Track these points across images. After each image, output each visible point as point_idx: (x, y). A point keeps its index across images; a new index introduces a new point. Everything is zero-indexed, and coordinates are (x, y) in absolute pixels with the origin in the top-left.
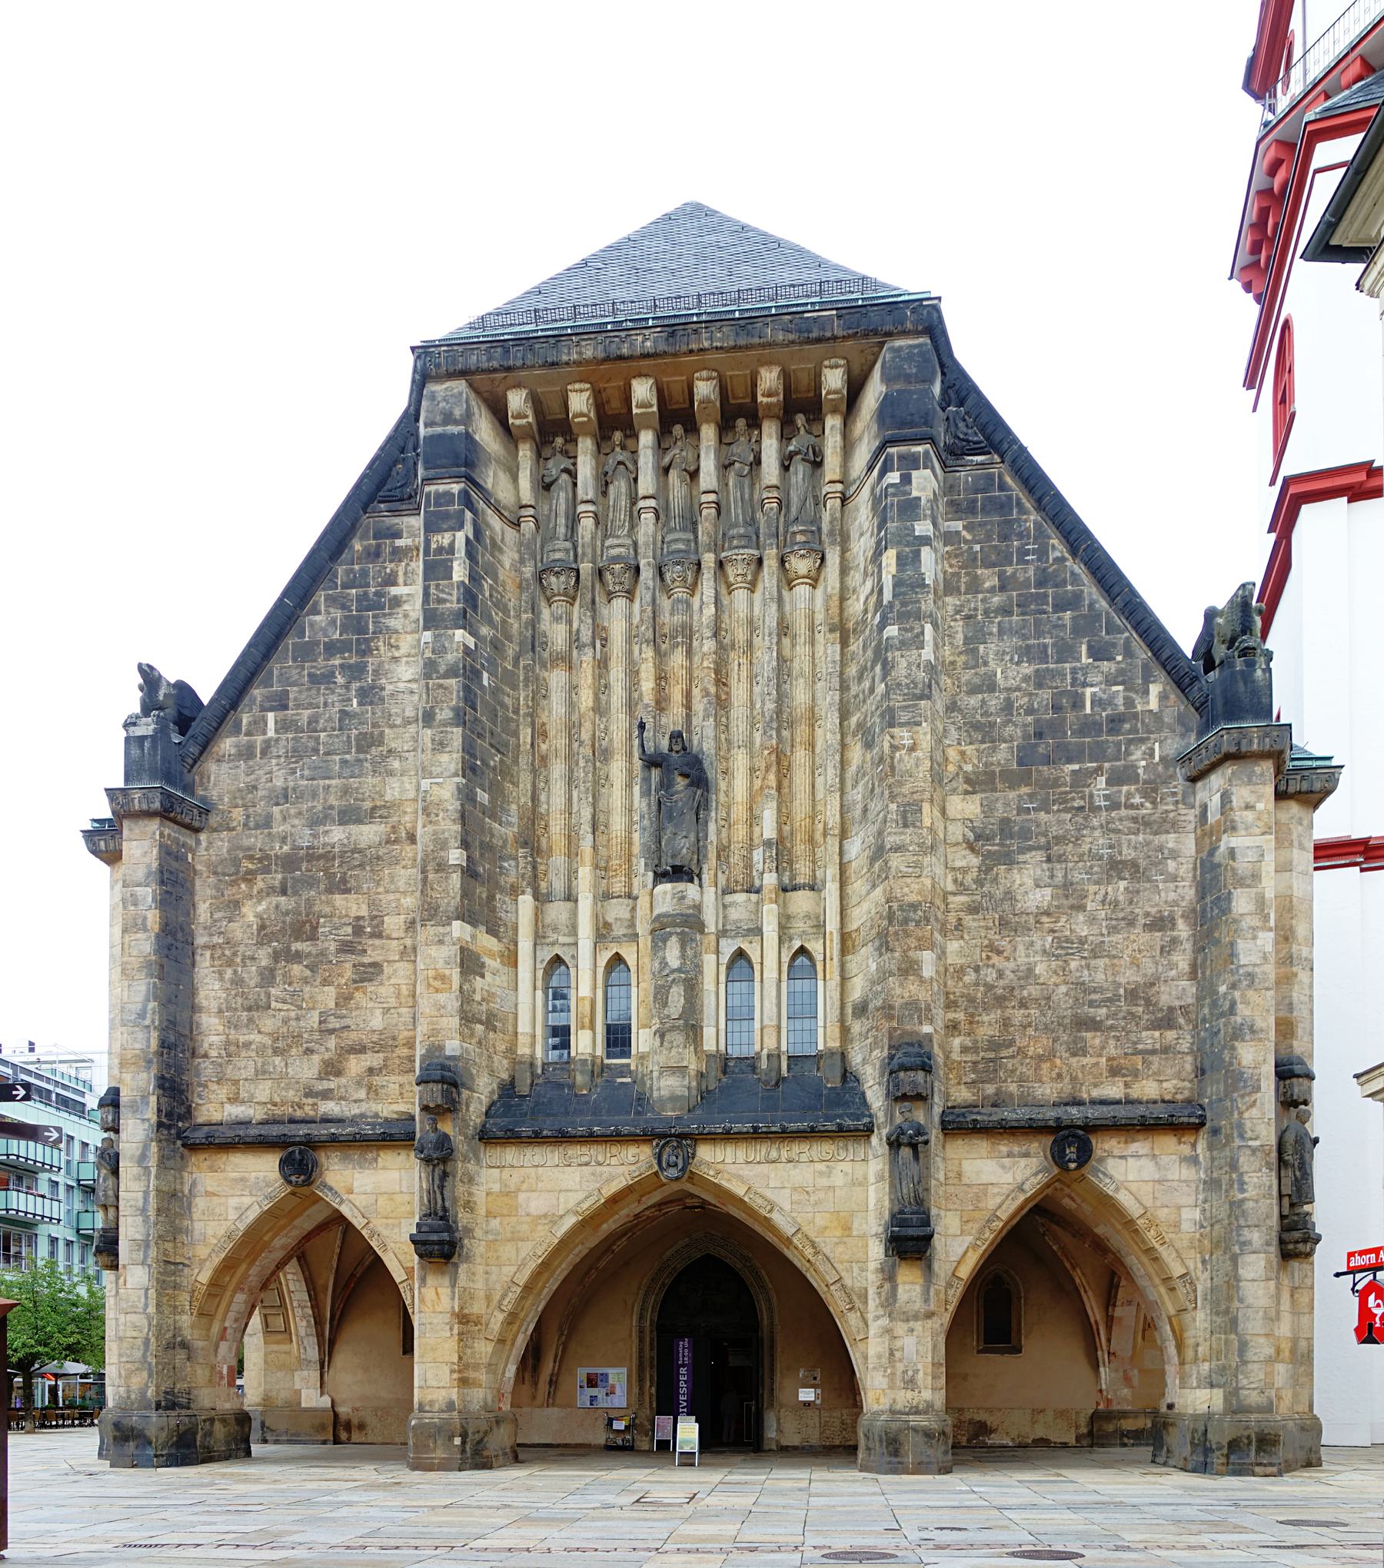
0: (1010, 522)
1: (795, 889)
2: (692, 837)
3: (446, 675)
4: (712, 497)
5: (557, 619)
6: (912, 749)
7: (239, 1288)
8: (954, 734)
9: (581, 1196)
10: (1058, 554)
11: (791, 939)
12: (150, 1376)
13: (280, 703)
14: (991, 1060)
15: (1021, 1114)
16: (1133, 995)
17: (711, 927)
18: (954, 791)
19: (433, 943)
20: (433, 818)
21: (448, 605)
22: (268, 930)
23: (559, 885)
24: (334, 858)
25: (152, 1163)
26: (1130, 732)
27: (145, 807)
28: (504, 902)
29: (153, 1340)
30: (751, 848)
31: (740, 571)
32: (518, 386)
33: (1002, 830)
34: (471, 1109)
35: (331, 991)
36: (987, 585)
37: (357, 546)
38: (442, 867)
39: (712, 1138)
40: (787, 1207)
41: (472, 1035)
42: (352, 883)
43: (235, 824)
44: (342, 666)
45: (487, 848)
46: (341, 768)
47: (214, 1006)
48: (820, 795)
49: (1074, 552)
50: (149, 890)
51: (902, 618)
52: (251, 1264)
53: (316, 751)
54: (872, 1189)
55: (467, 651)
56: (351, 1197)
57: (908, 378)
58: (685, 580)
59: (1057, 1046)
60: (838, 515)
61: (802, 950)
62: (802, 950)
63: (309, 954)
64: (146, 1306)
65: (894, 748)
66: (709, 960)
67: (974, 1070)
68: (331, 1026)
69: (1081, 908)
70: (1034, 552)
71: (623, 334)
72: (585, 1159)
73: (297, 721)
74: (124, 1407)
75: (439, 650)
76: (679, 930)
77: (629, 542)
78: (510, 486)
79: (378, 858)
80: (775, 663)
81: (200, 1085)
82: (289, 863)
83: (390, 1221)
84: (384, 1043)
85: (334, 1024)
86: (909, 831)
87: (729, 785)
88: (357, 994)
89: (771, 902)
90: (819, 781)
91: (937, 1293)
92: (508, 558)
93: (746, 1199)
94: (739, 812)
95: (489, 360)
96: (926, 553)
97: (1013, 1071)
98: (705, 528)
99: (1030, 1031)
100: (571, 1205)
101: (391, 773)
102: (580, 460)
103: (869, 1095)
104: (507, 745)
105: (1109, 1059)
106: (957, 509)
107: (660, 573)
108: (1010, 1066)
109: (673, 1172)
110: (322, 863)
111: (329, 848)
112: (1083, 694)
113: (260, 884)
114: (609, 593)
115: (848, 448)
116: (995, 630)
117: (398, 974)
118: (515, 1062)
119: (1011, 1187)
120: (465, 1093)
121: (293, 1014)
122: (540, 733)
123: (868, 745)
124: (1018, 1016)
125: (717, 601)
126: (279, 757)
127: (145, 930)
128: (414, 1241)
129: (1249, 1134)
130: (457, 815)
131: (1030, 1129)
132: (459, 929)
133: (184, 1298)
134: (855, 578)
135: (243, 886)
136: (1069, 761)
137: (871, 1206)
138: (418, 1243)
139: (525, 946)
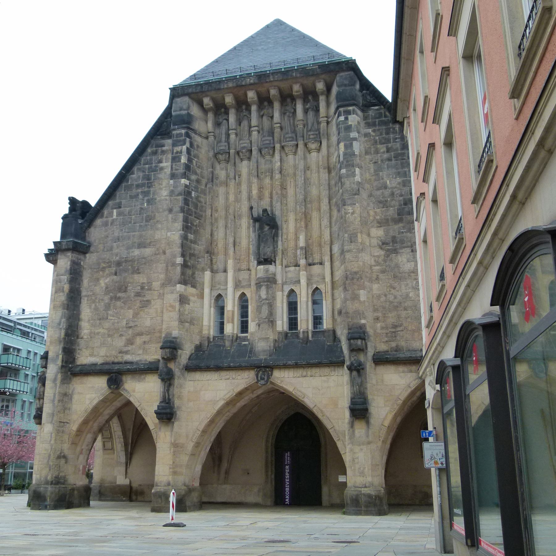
1: (314, 264)
2: (271, 248)
3: (178, 195)
4: (278, 125)
5: (222, 169)
6: (353, 213)
8: (371, 204)
11: (312, 284)
12: (50, 470)
14: (394, 332)
17: (279, 281)
18: (373, 227)
21: (179, 171)
23: (221, 266)
24: (135, 262)
25: (58, 382)
28: (199, 275)
29: (52, 455)
30: (296, 249)
31: (290, 149)
32: (207, 96)
33: (393, 241)
34: (182, 357)
35: (131, 312)
36: (382, 151)
38: (174, 264)
42: (141, 270)
44: (142, 192)
45: (192, 255)
51: (347, 166)
52: (94, 422)
53: (130, 222)
54: (345, 387)
55: (186, 186)
56: (134, 394)
57: (345, 85)
58: (269, 153)
60: (326, 128)
64: (51, 440)
65: (346, 213)
66: (279, 294)
67: (387, 336)
68: (130, 325)
70: (399, 138)
71: (243, 79)
72: (228, 377)
74: (38, 485)
76: (266, 284)
77: (248, 141)
79: (151, 260)
80: (303, 182)
82: (119, 264)
85: (131, 324)
87: (288, 226)
90: (322, 223)
94: (291, 236)
95: (196, 90)
96: (355, 143)
97: (403, 336)
98: (276, 135)
99: (409, 320)
101: (157, 229)
102: (230, 116)
104: (202, 216)
106: (368, 125)
107: (260, 151)
108: (401, 335)
109: (262, 382)
110: (130, 263)
111: (133, 258)
113: (107, 271)
114: (241, 159)
115: (328, 104)
116: (386, 166)
117: (156, 304)
120: (180, 352)
121: (116, 321)
122: (214, 210)
123: (339, 211)
126: (117, 225)
127: (63, 292)
128: (156, 412)
130: (179, 245)
133: (66, 437)
134: (332, 150)
135: (101, 273)
137: (345, 395)
139: (207, 291)
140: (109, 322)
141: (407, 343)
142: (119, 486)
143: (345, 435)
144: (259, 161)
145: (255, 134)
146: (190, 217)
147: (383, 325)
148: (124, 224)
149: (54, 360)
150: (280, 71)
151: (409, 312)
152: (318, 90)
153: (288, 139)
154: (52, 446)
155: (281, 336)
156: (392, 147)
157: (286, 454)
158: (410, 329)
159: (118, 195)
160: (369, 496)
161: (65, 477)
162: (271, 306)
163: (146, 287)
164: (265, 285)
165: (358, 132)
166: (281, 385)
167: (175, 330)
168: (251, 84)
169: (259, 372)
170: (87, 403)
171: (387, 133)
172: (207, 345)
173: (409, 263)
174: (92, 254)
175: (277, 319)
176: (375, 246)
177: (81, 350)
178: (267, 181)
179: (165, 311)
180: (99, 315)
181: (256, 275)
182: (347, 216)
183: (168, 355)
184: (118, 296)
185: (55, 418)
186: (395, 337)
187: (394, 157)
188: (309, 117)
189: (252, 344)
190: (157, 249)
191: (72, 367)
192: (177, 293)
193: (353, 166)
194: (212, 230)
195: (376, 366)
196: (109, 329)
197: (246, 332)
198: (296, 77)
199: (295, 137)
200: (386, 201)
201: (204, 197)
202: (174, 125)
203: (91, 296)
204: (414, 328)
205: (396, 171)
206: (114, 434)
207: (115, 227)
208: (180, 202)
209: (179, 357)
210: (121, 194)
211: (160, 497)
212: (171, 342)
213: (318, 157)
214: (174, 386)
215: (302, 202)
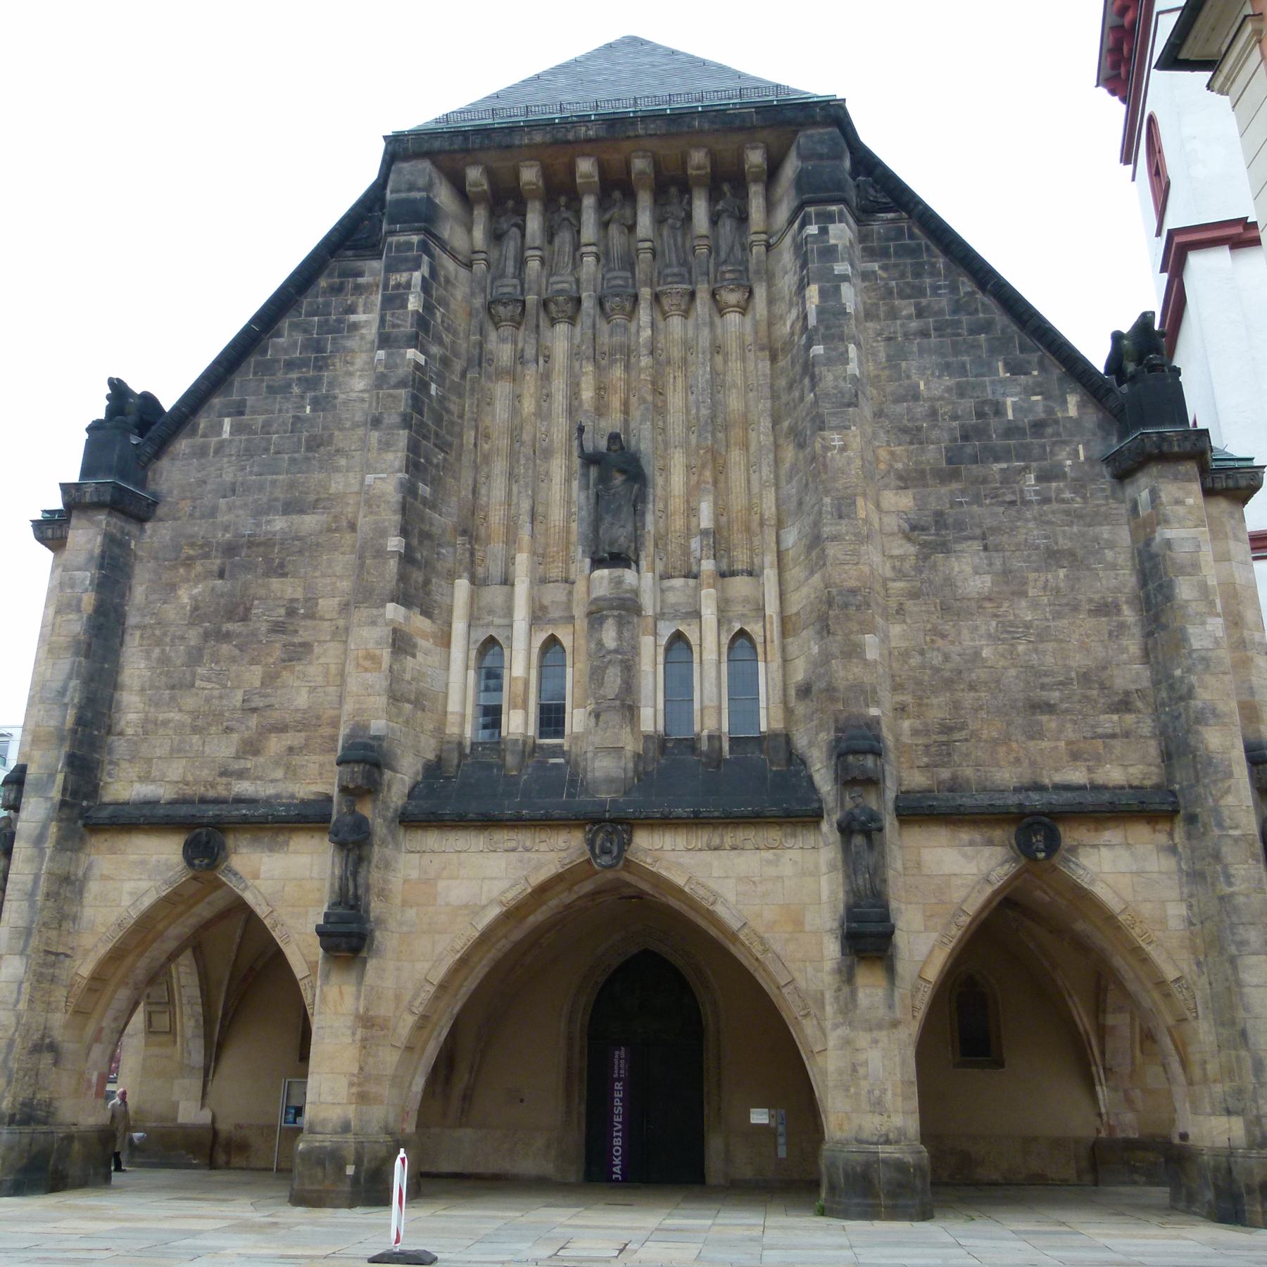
1: (733, 574)
2: (630, 528)
3: (396, 386)
4: (648, 244)
5: (503, 340)
6: (843, 449)
8: (883, 436)
9: (504, 884)
11: (730, 621)
12: (9, 1083)
14: (943, 743)
16: (1085, 678)
17: (649, 611)
18: (886, 487)
20: (375, 509)
21: (402, 329)
23: (496, 570)
24: (274, 545)
26: (1053, 436)
27: (95, 499)
28: (440, 586)
30: (688, 534)
31: (675, 302)
32: (476, 163)
33: (937, 522)
35: (258, 670)
36: (904, 313)
38: (381, 553)
40: (732, 898)
41: (399, 714)
42: (290, 568)
44: (299, 379)
45: (426, 536)
46: (289, 465)
48: (755, 490)
51: (826, 340)
52: (141, 955)
53: (267, 450)
55: (417, 366)
56: (257, 882)
58: (623, 308)
62: (742, 633)
63: (239, 635)
64: (17, 1001)
65: (826, 448)
66: (647, 642)
67: (927, 753)
68: (253, 705)
69: (1023, 594)
70: (945, 287)
71: (569, 126)
72: (512, 844)
76: (616, 613)
77: (572, 279)
78: (465, 237)
79: (318, 545)
82: (230, 550)
84: (308, 722)
85: (258, 702)
86: (844, 522)
87: (667, 481)
93: (687, 889)
94: (677, 504)
95: (451, 144)
97: (967, 755)
99: (983, 714)
100: (495, 893)
101: (337, 470)
104: (450, 445)
105: (1069, 743)
106: (870, 253)
107: (601, 302)
108: (964, 749)
109: (606, 860)
110: (262, 549)
111: (270, 536)
112: (1005, 403)
113: (198, 568)
115: (770, 207)
116: (915, 349)
117: (327, 655)
120: (388, 774)
121: (216, 693)
124: (968, 699)
125: (653, 325)
126: (231, 455)
127: (79, 610)
128: (320, 931)
129: (1228, 822)
130: (397, 507)
132: (393, 611)
133: (60, 994)
135: (182, 570)
136: (997, 459)
139: (459, 627)
140: (197, 694)
141: (978, 770)
142: (183, 1127)
143: (823, 1003)
144: (598, 326)
145: (589, 261)
146: (424, 442)
147: (918, 724)
148: (248, 452)
149: (42, 787)
150: (663, 113)
151: (983, 694)
152: (750, 167)
153: (669, 279)
154: (19, 1017)
155: (651, 746)
156: (929, 306)
157: (617, 1053)
158: (984, 737)
159: (236, 384)
160: (900, 1166)
161: (49, 1104)
162: (629, 668)
163: (302, 611)
164: (614, 616)
165: (852, 266)
166: (654, 870)
167: (378, 718)
168: (589, 140)
169: (595, 834)
170: (123, 904)
171: (917, 275)
172: (455, 762)
173: (977, 577)
174: (160, 524)
175: (643, 703)
176: (893, 534)
177: (117, 764)
178: (618, 372)
179: (350, 668)
180: (171, 677)
181: (588, 592)
182: (829, 454)
183: (360, 781)
184: (224, 629)
185: (34, 942)
186: (949, 754)
187: (935, 329)
188: (722, 231)
189: (577, 764)
190: (335, 517)
191: (89, 808)
192: (387, 625)
193: (841, 339)
194: (475, 481)
195: (901, 827)
196: (195, 715)
197: (559, 733)
198: (701, 132)
199: (687, 276)
200: (919, 429)
201: (457, 400)
202: (392, 221)
203: (151, 626)
204: (995, 734)
205: (939, 360)
206: (180, 993)
207: (225, 460)
208: (403, 403)
209: (386, 789)
210: (245, 381)
211: (321, 1163)
212: (366, 747)
213: (742, 324)
214: (370, 862)
215: (706, 423)
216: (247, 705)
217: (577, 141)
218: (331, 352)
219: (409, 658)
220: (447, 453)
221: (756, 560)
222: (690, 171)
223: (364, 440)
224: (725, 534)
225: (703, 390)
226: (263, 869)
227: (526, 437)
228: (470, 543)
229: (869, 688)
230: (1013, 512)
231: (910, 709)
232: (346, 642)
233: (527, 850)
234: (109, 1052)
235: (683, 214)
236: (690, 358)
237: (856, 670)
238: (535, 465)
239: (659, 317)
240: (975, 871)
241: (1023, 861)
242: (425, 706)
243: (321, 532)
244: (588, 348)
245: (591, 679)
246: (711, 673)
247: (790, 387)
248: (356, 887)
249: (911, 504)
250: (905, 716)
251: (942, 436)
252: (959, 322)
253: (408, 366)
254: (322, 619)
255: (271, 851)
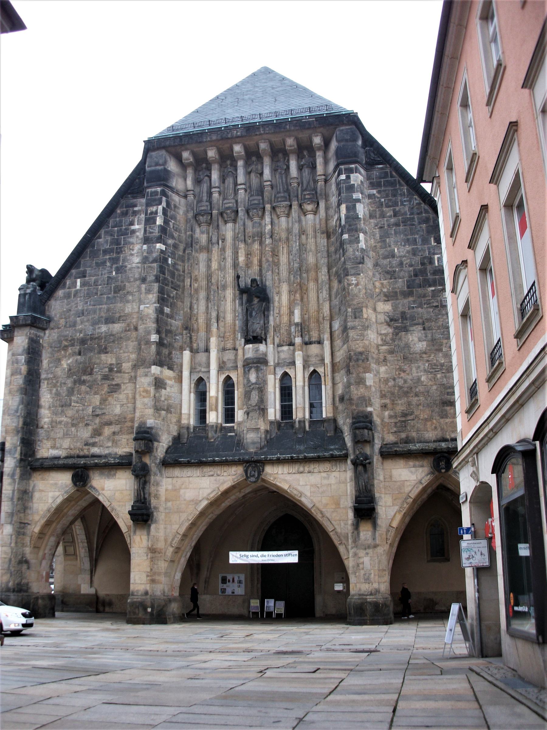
0: (396, 190)
1: (311, 343)
2: (262, 322)
4: (269, 183)
5: (202, 233)
6: (357, 285)
7: (52, 535)
8: (378, 276)
9: (209, 491)
10: (417, 202)
11: (309, 367)
12: (11, 576)
13: (83, 275)
15: (418, 446)
17: (271, 363)
18: (379, 300)
19: (143, 376)
20: (145, 322)
22: (72, 371)
23: (202, 345)
24: (102, 339)
25: (17, 477)
27: (24, 323)
28: (177, 354)
30: (290, 325)
31: (282, 210)
32: (186, 149)
33: (402, 317)
36: (388, 214)
37: (119, 211)
38: (148, 342)
39: (273, 462)
40: (308, 494)
41: (160, 416)
42: (109, 349)
43: (61, 326)
44: (109, 258)
45: (168, 332)
46: (107, 300)
47: (47, 405)
48: (321, 302)
49: (424, 201)
50: (23, 357)
51: (349, 231)
53: (96, 294)
55: (162, 251)
56: (104, 492)
58: (258, 215)
59: (434, 414)
60: (323, 187)
61: (315, 371)
62: (315, 371)
63: (89, 381)
64: (11, 543)
65: (349, 285)
67: (395, 426)
68: (97, 413)
69: (440, 350)
71: (228, 131)
72: (211, 473)
73: (89, 282)
75: (150, 252)
76: (255, 365)
77: (233, 201)
78: (183, 183)
79: (121, 338)
81: (39, 441)
82: (83, 342)
83: (121, 504)
84: (120, 420)
85: (99, 412)
86: (357, 320)
87: (280, 298)
88: (110, 399)
89: (299, 350)
90: (320, 295)
91: (381, 535)
92: (181, 211)
93: (288, 491)
94: (285, 310)
95: (174, 143)
97: (414, 426)
100: (205, 495)
101: (128, 302)
102: (213, 172)
103: (346, 439)
107: (247, 212)
108: (412, 424)
109: (253, 479)
111: (100, 335)
112: (434, 258)
113: (70, 351)
115: (326, 162)
116: (393, 232)
117: (127, 390)
118: (181, 427)
119: (416, 482)
120: (156, 444)
121: (81, 408)
123: (340, 282)
125: (272, 223)
126: (81, 297)
127: (21, 374)
128: (130, 513)
130: (155, 320)
131: (423, 454)
132: (155, 369)
133: (27, 540)
134: (331, 212)
135: (63, 352)
138: (131, 514)
139: (186, 373)
143: (348, 538)
145: (241, 192)
146: (166, 287)
147: (392, 413)
148: (89, 295)
151: (421, 398)
154: (12, 549)
156: (399, 211)
158: (421, 418)
159: (82, 263)
161: (27, 584)
166: (274, 483)
168: (238, 137)
174: (52, 331)
175: (269, 406)
176: (382, 323)
178: (256, 246)
179: (137, 396)
185: (15, 518)
192: (152, 376)
197: (233, 421)
201: (182, 264)
204: (426, 416)
206: (77, 538)
209: (155, 450)
210: (86, 260)
212: (146, 432)
213: (315, 220)
214: (150, 483)
215: (297, 271)
216: (94, 413)
217: (232, 138)
218: (124, 244)
219: (163, 390)
220: (177, 290)
221: (321, 336)
222: (287, 148)
223: (139, 287)
224: (307, 324)
225: (295, 254)
226: (106, 486)
227: (213, 281)
228: (189, 333)
229: (367, 398)
230: (437, 311)
231: (389, 406)
232: (135, 383)
233: (218, 475)
234: (49, 563)
235: (285, 167)
236: (290, 237)
237: (362, 390)
238: (218, 294)
239: (275, 217)
240: (415, 478)
241: (437, 473)
242: (171, 411)
243: (122, 332)
244: (241, 236)
245: (245, 396)
246: (300, 391)
247: (336, 252)
248: (144, 494)
249: (391, 308)
250: (386, 409)
251: (405, 274)
252: (413, 218)
253: (157, 252)
254: (124, 373)
255: (108, 478)
